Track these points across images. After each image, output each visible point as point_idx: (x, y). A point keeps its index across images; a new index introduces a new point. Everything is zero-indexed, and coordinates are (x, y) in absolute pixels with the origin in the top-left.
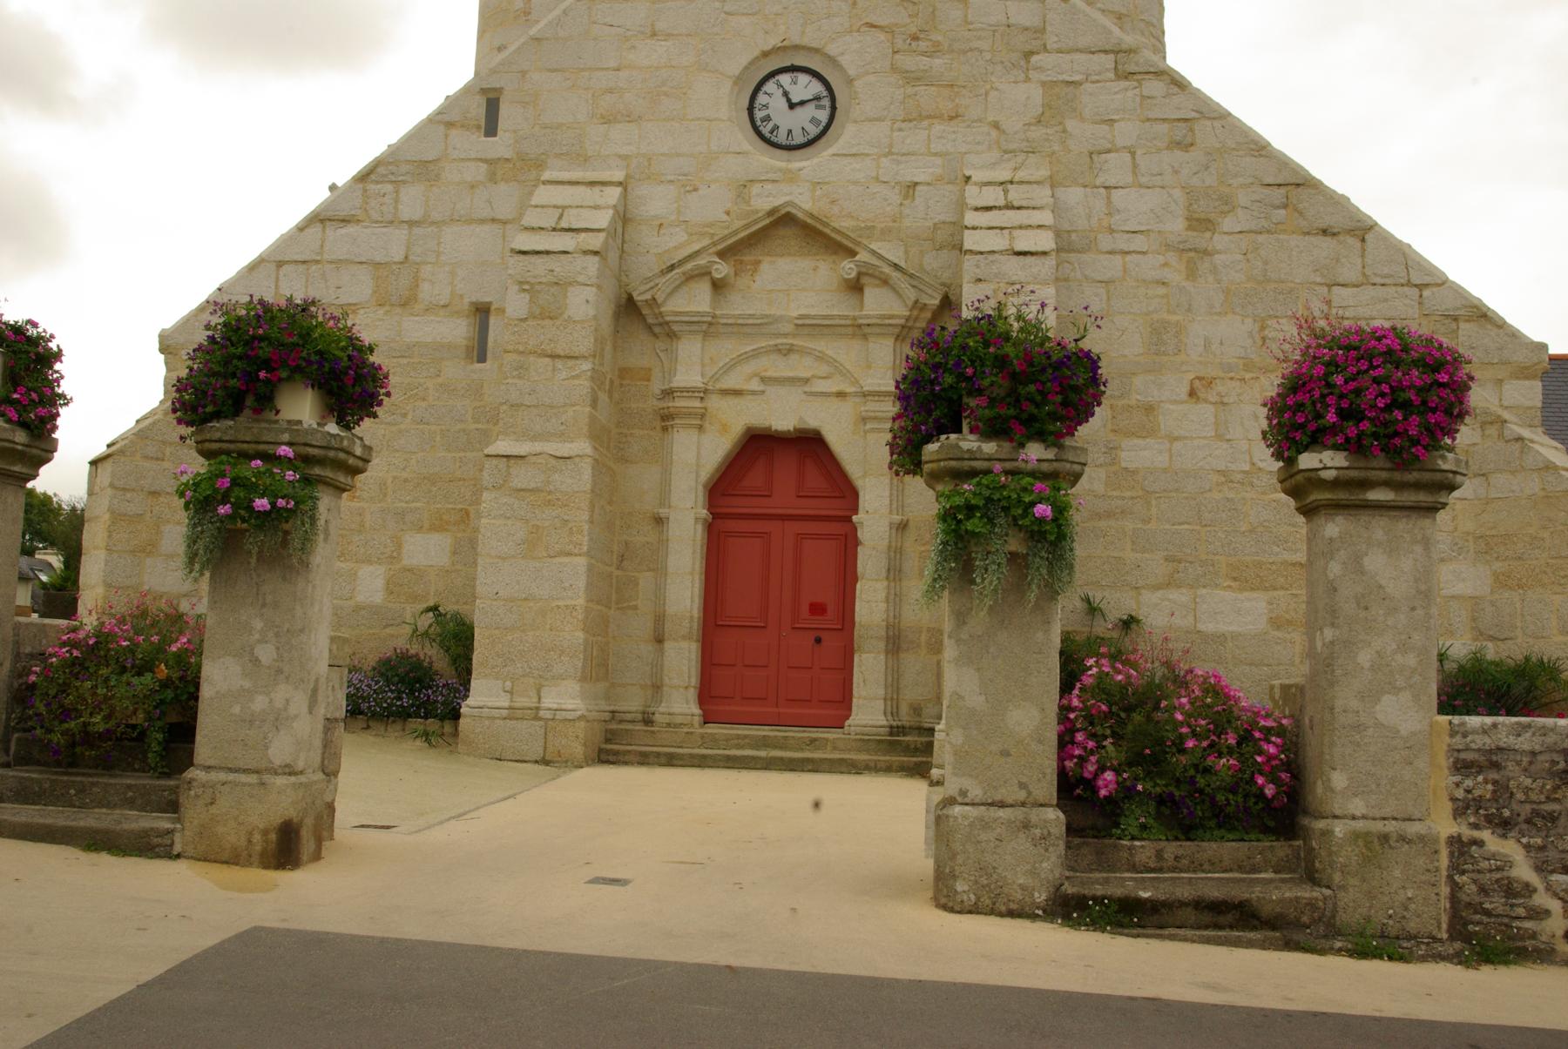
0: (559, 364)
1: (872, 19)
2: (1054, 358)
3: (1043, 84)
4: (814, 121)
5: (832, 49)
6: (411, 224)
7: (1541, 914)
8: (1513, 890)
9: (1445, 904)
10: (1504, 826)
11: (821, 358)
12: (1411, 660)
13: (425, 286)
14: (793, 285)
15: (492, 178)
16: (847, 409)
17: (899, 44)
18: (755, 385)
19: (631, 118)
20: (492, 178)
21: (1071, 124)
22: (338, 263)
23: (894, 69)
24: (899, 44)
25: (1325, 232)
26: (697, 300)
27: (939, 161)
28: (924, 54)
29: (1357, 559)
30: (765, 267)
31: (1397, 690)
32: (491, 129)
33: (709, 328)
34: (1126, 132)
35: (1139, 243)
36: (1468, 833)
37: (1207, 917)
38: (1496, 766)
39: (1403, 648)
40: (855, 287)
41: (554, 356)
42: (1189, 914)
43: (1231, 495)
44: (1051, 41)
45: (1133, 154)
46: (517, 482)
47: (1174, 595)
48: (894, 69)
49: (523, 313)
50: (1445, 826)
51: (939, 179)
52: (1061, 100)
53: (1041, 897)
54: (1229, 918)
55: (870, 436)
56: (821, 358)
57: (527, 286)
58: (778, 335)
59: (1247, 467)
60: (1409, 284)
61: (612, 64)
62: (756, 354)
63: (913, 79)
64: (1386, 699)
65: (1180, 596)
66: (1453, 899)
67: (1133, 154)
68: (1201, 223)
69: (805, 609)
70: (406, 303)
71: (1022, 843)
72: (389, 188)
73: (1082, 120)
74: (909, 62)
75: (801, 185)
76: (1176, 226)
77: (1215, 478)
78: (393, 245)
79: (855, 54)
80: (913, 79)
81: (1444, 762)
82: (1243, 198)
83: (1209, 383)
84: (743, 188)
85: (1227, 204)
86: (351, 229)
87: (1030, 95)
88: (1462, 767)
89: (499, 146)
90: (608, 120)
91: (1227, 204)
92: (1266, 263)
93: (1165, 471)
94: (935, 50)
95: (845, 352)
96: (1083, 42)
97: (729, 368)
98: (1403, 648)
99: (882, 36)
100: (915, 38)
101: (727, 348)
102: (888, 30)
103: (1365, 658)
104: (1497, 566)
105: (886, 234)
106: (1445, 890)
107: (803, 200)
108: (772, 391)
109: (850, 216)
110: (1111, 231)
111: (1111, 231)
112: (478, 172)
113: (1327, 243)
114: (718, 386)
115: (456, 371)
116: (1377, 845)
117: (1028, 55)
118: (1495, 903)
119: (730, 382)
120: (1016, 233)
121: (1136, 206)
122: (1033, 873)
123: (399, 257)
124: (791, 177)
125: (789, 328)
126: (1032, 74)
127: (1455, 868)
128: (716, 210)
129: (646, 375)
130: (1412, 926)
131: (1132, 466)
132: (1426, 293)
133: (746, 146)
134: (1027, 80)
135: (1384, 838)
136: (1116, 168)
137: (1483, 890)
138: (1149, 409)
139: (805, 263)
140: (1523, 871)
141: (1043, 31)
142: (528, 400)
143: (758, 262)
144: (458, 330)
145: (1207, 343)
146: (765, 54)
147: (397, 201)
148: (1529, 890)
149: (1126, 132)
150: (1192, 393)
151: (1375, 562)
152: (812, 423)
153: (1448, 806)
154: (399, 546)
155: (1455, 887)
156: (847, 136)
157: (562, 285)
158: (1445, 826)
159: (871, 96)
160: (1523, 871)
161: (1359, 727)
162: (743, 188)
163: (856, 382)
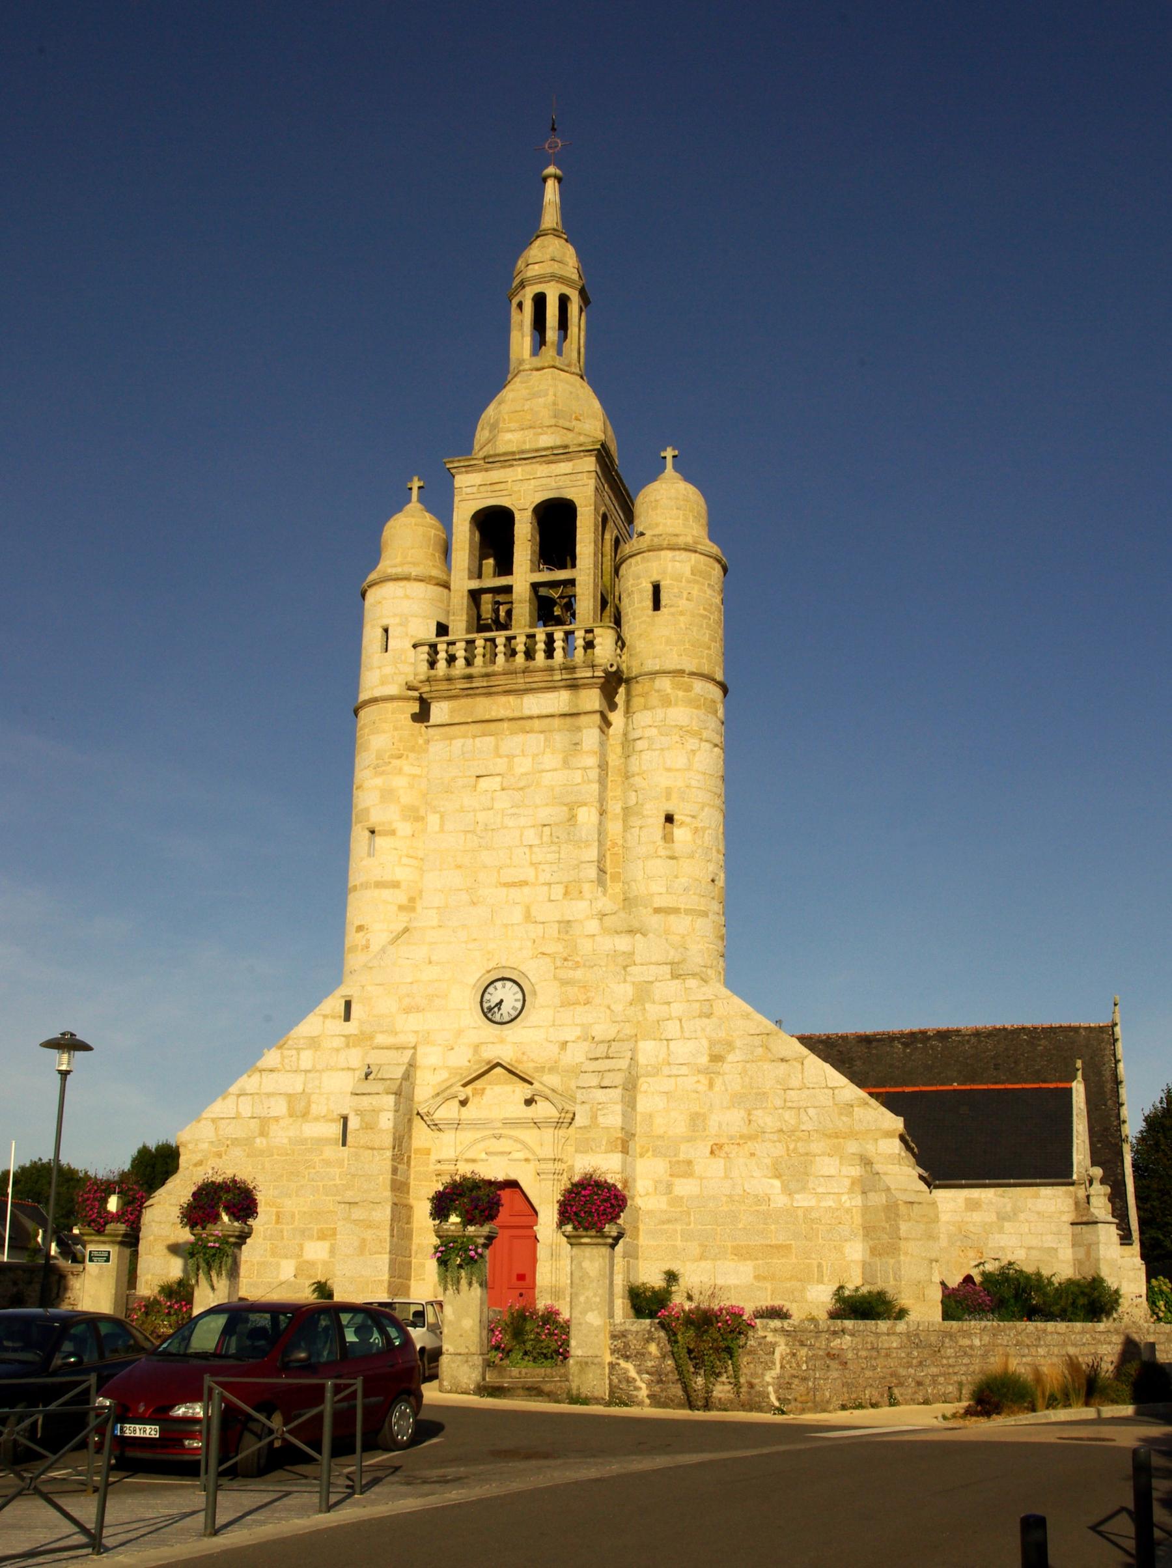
0: (375, 1152)
1: (544, 950)
2: (273, 1270)
3: (633, 983)
4: (514, 1008)
5: (522, 968)
6: (306, 1071)
7: (638, 1389)
8: (630, 1381)
9: (607, 1386)
10: (627, 1358)
11: (517, 1140)
12: (598, 1299)
13: (314, 1106)
14: (501, 1099)
15: (348, 1046)
16: (531, 1167)
17: (559, 964)
18: (483, 1156)
19: (418, 1009)
20: (348, 1046)
21: (647, 1006)
22: (269, 1095)
23: (555, 978)
24: (559, 964)
25: (782, 1060)
26: (449, 1111)
27: (579, 1029)
28: (571, 968)
29: (580, 1263)
30: (488, 1092)
31: (593, 1310)
32: (347, 1018)
33: (458, 1125)
34: (677, 1009)
35: (684, 1070)
36: (615, 1361)
37: (527, 1393)
38: (624, 1336)
39: (595, 1295)
40: (529, 1102)
41: (373, 1149)
42: (521, 1392)
43: (734, 1208)
44: (638, 959)
45: (681, 1021)
46: (354, 1217)
47: (703, 1264)
48: (555, 978)
49: (357, 1127)
50: (608, 1358)
51: (579, 1038)
52: (643, 993)
53: (472, 1387)
54: (534, 1392)
55: (543, 1183)
56: (517, 1140)
57: (359, 1112)
58: (494, 1129)
59: (741, 1192)
60: (827, 1087)
61: (409, 980)
62: (484, 1139)
63: (565, 983)
64: (590, 1314)
65: (706, 1265)
66: (610, 1384)
67: (681, 1021)
68: (716, 1058)
69: (514, 1277)
70: (305, 1115)
71: (465, 1368)
72: (294, 1052)
73: (654, 1002)
74: (562, 974)
75: (505, 1045)
76: (704, 1060)
77: (724, 1199)
78: (296, 1084)
79: (535, 971)
80: (565, 983)
81: (608, 1336)
82: (738, 1043)
83: (720, 1146)
84: (476, 1048)
85: (730, 1045)
86: (274, 1075)
87: (625, 991)
88: (614, 1337)
89: (352, 1027)
90: (407, 1011)
91: (730, 1045)
92: (751, 1078)
93: (698, 1197)
94: (577, 966)
95: (529, 1136)
96: (653, 960)
97: (470, 1146)
98: (595, 1295)
99: (548, 960)
100: (566, 960)
101: (467, 1136)
102: (551, 956)
103: (582, 1299)
104: (871, 1243)
105: (552, 1070)
106: (607, 1382)
107: (505, 1054)
108: (492, 1159)
109: (532, 1061)
110: (669, 1064)
111: (669, 1064)
112: (339, 1042)
113: (784, 1065)
114: (465, 1157)
115: (334, 1152)
116: (584, 1364)
117: (625, 968)
118: (623, 1386)
119: (469, 1155)
120: (606, 1074)
121: (681, 1050)
122: (469, 1378)
123: (300, 1090)
124: (502, 1041)
125: (500, 1125)
126: (628, 978)
127: (611, 1373)
128: (463, 1060)
129: (428, 1152)
130: (596, 1394)
131: (681, 1194)
132: (836, 1092)
133: (480, 1023)
134: (625, 981)
135: (586, 1363)
136: (672, 1029)
137: (620, 1381)
138: (689, 1163)
139: (508, 1088)
140: (633, 1373)
141: (633, 953)
142: (360, 1173)
143: (484, 1089)
144: (336, 1130)
145: (720, 1126)
146: (489, 972)
147: (298, 1059)
148: (634, 1380)
149: (677, 1009)
150: (712, 1152)
151: (586, 1264)
152: (513, 1176)
153: (609, 1351)
154: (302, 1249)
155: (611, 1380)
156: (533, 1016)
157: (376, 1111)
158: (608, 1358)
159: (545, 994)
160: (633, 1373)
161: (580, 1324)
162: (476, 1048)
163: (534, 1153)
